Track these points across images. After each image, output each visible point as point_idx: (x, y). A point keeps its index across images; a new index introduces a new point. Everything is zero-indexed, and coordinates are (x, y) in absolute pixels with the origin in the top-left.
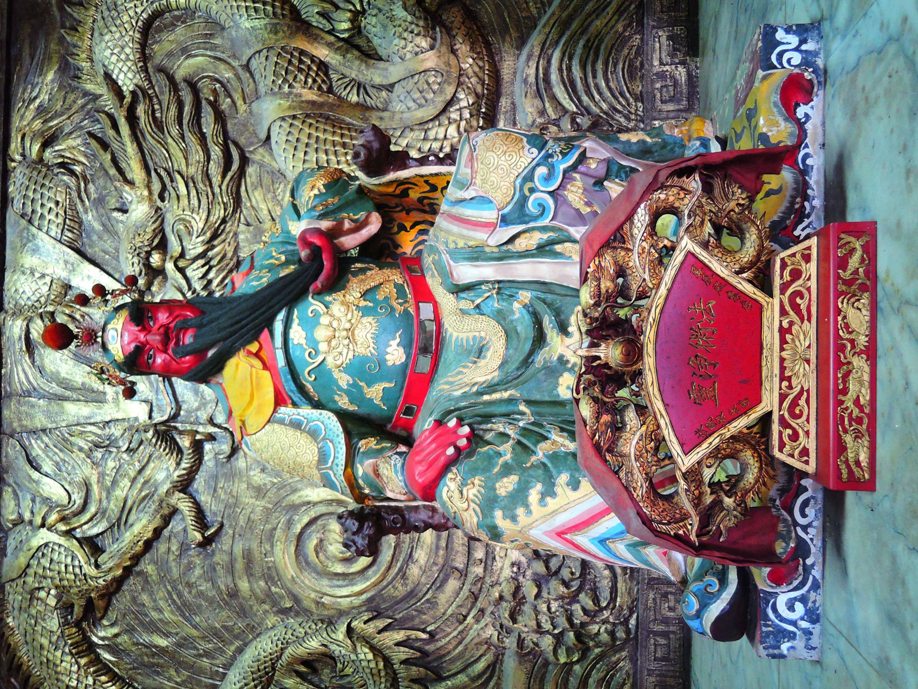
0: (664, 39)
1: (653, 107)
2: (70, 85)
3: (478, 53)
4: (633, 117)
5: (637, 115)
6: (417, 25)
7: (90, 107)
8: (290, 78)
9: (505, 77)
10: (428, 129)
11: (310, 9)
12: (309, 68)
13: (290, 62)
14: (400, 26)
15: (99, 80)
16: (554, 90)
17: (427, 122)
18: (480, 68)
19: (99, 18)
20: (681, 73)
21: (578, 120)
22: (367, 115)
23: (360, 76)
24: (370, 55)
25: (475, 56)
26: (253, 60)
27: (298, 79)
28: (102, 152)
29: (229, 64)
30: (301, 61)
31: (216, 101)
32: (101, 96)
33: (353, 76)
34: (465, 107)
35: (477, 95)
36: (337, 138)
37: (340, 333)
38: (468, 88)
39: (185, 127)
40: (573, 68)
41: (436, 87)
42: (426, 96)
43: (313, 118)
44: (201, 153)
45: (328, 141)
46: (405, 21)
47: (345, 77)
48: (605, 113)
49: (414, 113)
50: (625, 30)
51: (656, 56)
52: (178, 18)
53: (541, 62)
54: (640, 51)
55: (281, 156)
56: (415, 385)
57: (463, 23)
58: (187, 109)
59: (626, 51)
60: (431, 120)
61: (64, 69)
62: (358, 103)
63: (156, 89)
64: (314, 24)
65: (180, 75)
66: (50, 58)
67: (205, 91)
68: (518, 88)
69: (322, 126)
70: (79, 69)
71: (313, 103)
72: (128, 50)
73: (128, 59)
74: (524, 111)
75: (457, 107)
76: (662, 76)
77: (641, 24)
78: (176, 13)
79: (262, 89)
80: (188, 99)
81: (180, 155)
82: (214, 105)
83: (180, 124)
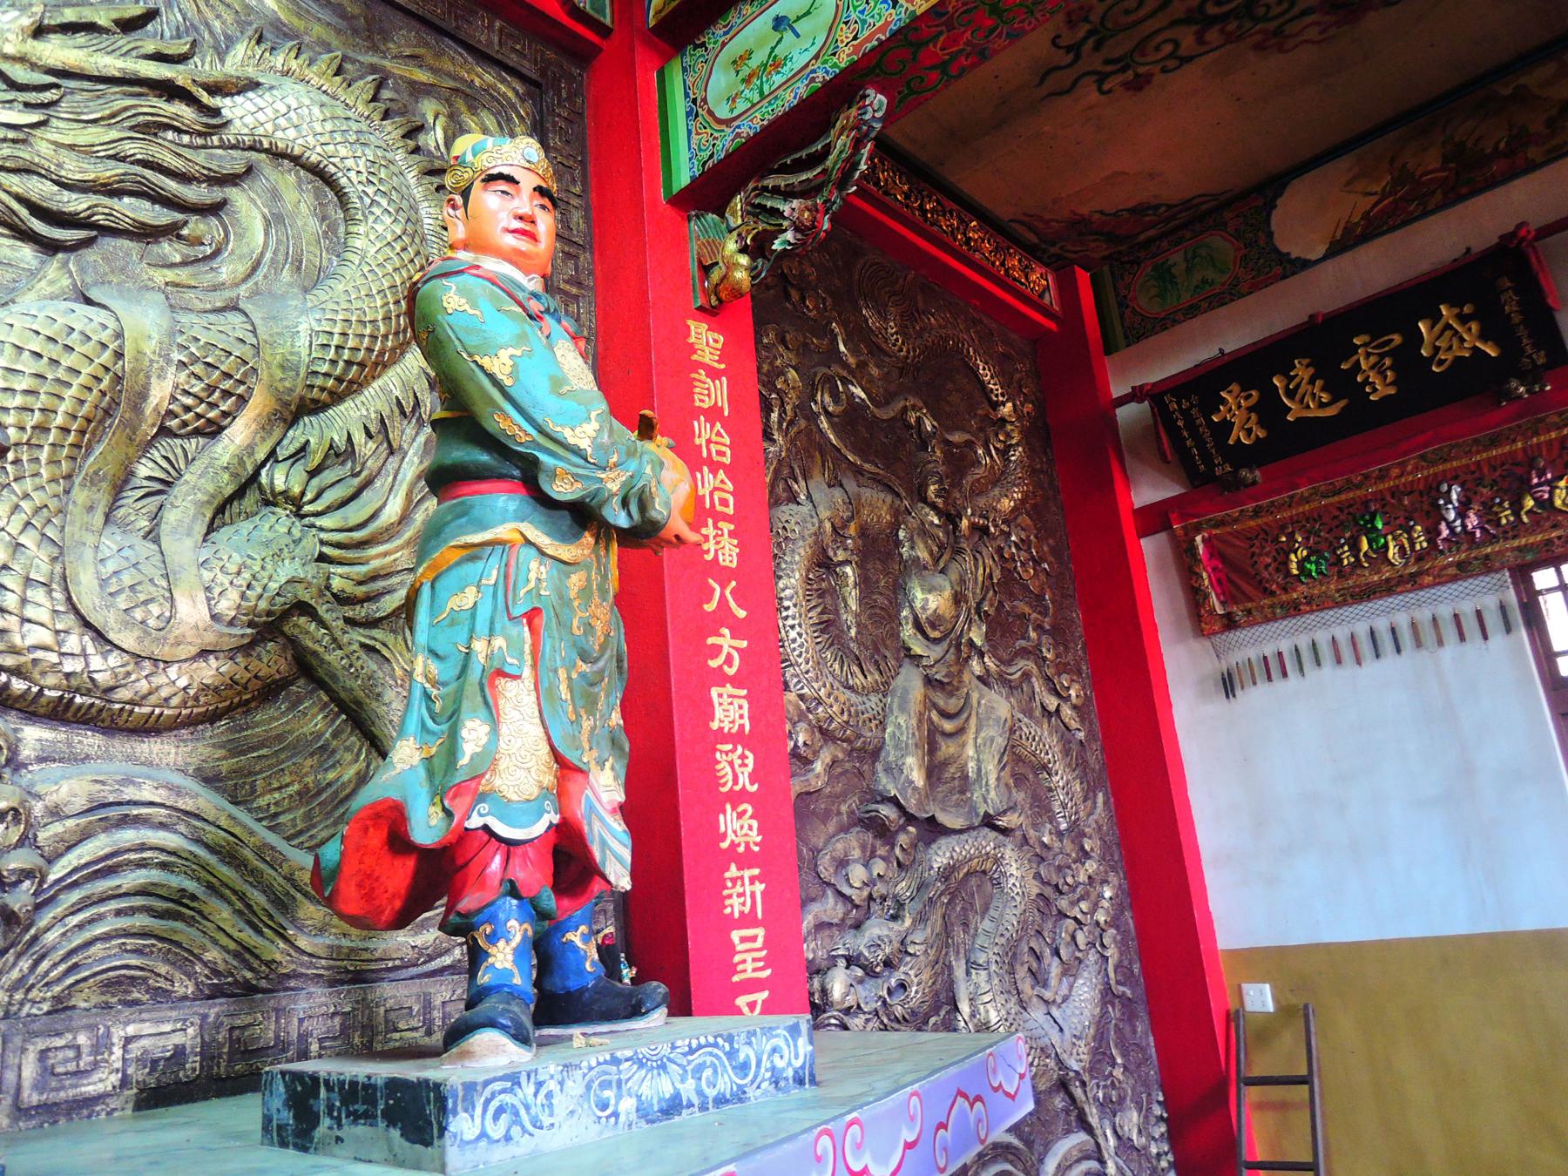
0: (178, 1039)
1: (33, 1035)
2: (250, 24)
3: (196, 699)
4: (18, 996)
5: (22, 1004)
6: (260, 597)
7: (207, 36)
8: (198, 369)
9: (145, 746)
10: (50, 591)
11: (316, 432)
12: (213, 406)
13: (227, 376)
14: (263, 568)
15: (250, 70)
16: (102, 836)
17: (67, 589)
18: (166, 700)
19: (350, 114)
20: (102, 1082)
21: (27, 883)
22: (104, 485)
23: (184, 488)
24: (221, 512)
25: (192, 692)
26: (242, 318)
27: (193, 381)
28: (115, 15)
29: (244, 280)
30: (227, 394)
31: (179, 237)
32: (222, 61)
33: (187, 477)
34: (87, 665)
35: (112, 689)
36: (59, 420)
38: (128, 674)
39: (138, 169)
40: (144, 872)
41: (138, 614)
42: (123, 596)
43: (112, 388)
44: (78, 177)
45: (56, 401)
46: (270, 578)
47: (188, 462)
48: (35, 939)
49: (91, 570)
50: (205, 964)
51: (147, 1028)
52: (332, 228)
53: (163, 811)
54: (162, 996)
55: (40, 310)
57: (256, 677)
58: (172, 185)
59: (163, 969)
60: (69, 599)
61: (277, 28)
62: (132, 474)
63: (220, 151)
64: (291, 433)
65: (237, 196)
66: (299, 16)
67: (201, 226)
68: (119, 768)
69: (91, 398)
70: (273, 49)
71: (143, 395)
72: (291, 133)
73: (277, 128)
74: (64, 778)
75: (90, 649)
76: (101, 1045)
77: (216, 993)
78: (342, 229)
79: (185, 319)
80: (191, 193)
81: (81, 140)
82: (171, 231)
83: (145, 164)
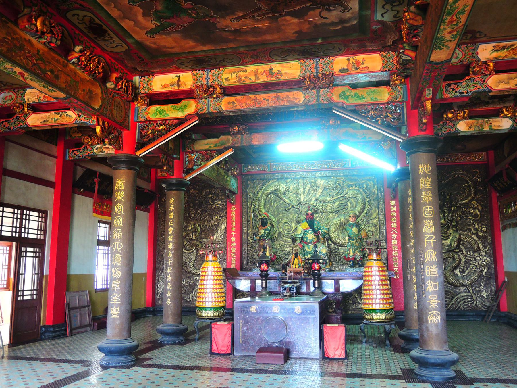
37: (310, 236)
56: (306, 243)
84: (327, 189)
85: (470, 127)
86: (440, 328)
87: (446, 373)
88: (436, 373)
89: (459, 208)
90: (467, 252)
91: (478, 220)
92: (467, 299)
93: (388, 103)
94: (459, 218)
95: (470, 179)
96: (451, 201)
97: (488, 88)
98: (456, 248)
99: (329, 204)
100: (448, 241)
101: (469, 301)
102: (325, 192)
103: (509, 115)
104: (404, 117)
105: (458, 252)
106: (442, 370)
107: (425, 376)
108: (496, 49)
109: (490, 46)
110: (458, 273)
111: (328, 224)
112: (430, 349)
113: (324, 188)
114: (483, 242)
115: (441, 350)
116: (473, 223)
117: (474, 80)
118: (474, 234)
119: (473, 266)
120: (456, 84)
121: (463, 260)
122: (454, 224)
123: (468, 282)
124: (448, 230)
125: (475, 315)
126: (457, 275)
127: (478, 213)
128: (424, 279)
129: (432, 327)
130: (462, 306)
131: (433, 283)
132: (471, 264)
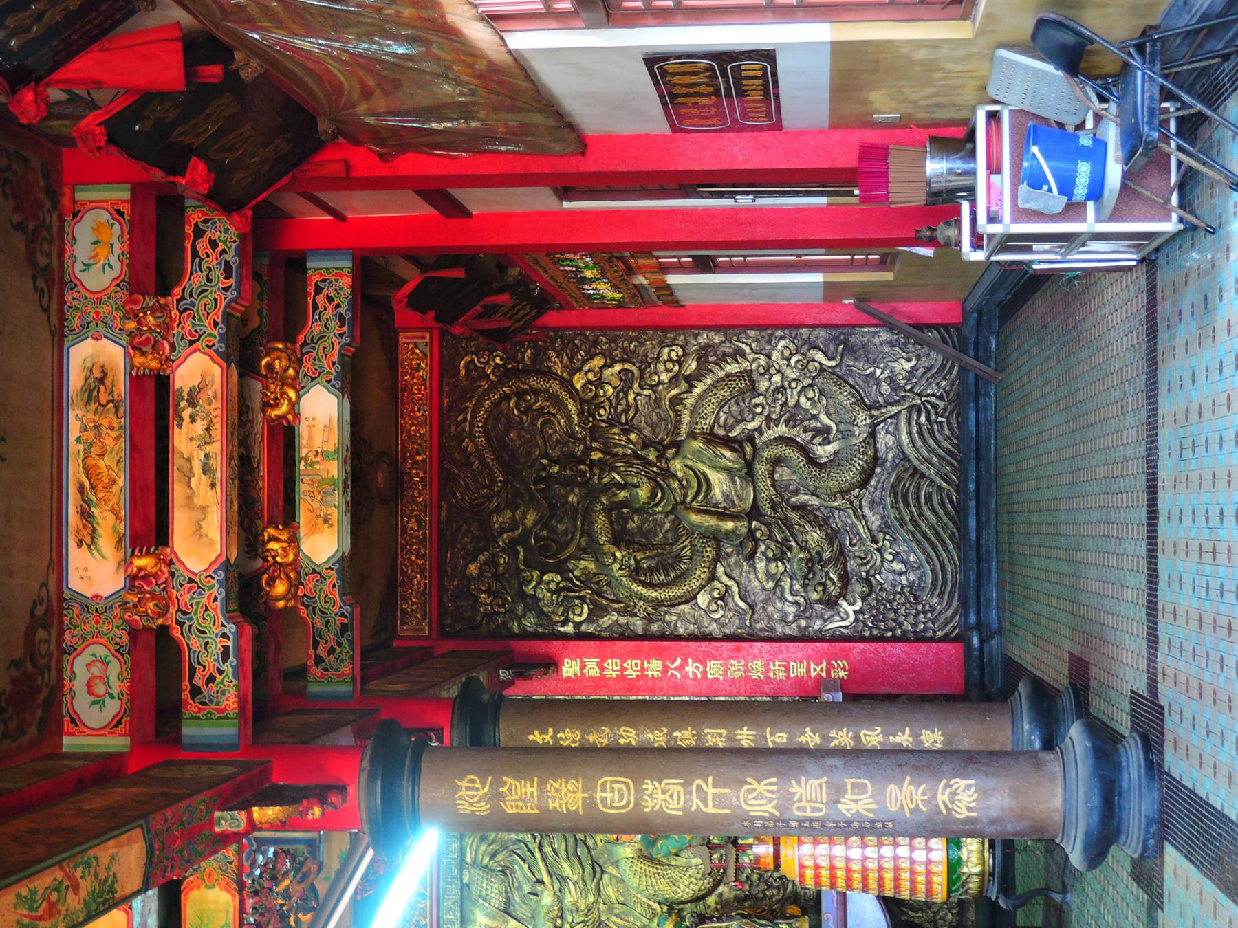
84: (508, 901)
85: (326, 521)
86: (991, 782)
87: (1134, 775)
88: (1134, 806)
89: (594, 433)
90: (755, 414)
91: (642, 371)
92: (919, 425)
93: (241, 886)
94: (633, 436)
95: (493, 387)
96: (570, 460)
97: (215, 572)
98: (740, 451)
99: (568, 899)
100: (715, 477)
101: (928, 418)
102: (520, 909)
103: (292, 394)
104: (295, 841)
105: (754, 445)
106: (1125, 784)
107: (1145, 841)
108: (89, 539)
109: (76, 557)
110: (830, 448)
111: (643, 904)
112: (1058, 817)
113: (506, 912)
114: (722, 359)
115: (1060, 783)
116: (652, 387)
117: (185, 613)
118: (692, 386)
119: (803, 400)
120: (193, 671)
121: (781, 430)
122: (652, 456)
123: (863, 418)
124: (675, 477)
125: (977, 402)
126: (836, 453)
127: (618, 367)
128: (835, 822)
129: (988, 807)
130: (946, 444)
131: (849, 796)
132: (797, 403)
